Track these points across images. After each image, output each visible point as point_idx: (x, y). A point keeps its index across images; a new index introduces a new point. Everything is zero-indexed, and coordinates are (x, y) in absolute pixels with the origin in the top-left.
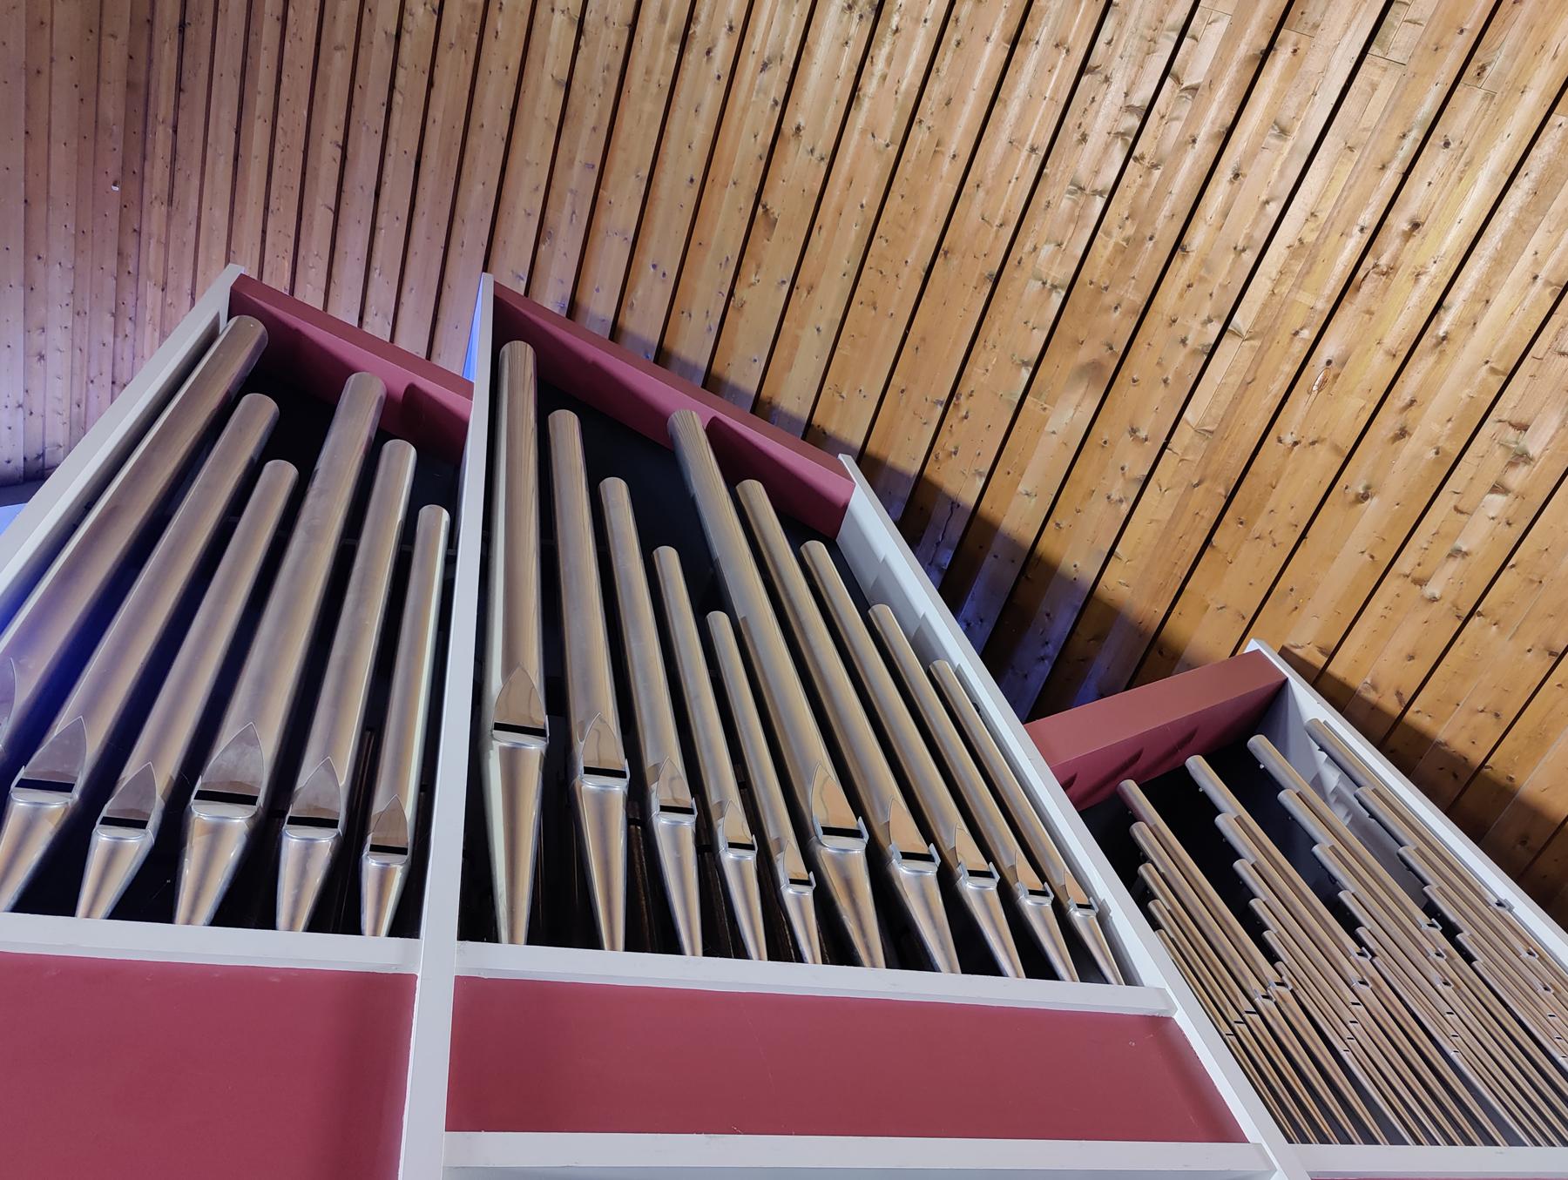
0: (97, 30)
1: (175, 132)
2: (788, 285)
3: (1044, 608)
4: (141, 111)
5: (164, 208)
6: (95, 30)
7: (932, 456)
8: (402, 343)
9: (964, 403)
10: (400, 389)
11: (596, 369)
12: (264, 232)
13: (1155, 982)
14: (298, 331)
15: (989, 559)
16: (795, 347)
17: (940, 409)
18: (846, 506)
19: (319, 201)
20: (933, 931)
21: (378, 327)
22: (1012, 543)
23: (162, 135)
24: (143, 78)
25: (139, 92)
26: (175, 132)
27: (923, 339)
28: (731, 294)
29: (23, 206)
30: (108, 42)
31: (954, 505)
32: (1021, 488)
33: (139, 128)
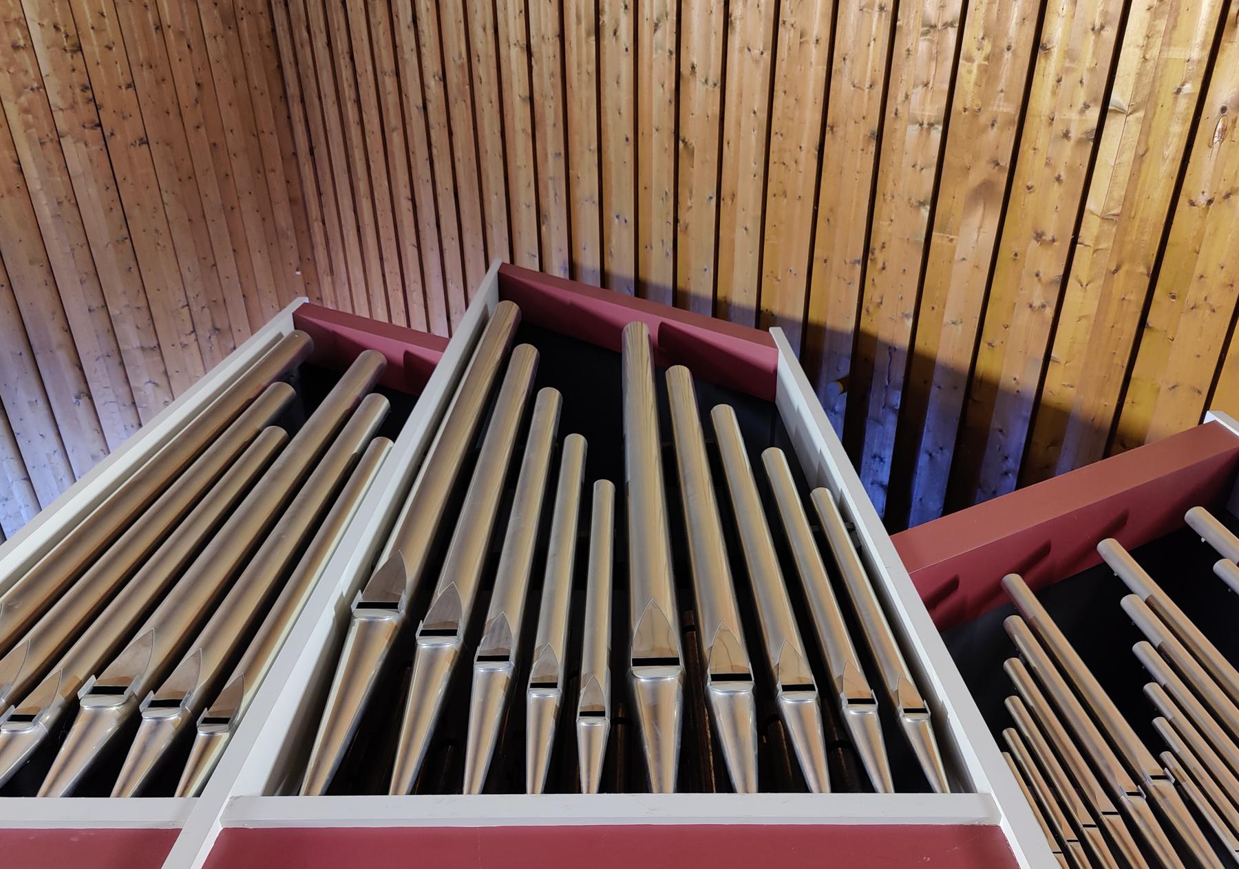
1: (324, 224)
3: (995, 424)
6: (261, 170)
7: (864, 311)
9: (879, 256)
10: (399, 357)
12: (384, 276)
14: (334, 334)
15: (934, 391)
17: (859, 267)
18: (775, 371)
21: (381, 316)
22: (951, 372)
23: (317, 227)
24: (300, 194)
26: (324, 224)
27: (831, 210)
28: (676, 221)
30: (270, 175)
31: (891, 349)
33: (304, 227)
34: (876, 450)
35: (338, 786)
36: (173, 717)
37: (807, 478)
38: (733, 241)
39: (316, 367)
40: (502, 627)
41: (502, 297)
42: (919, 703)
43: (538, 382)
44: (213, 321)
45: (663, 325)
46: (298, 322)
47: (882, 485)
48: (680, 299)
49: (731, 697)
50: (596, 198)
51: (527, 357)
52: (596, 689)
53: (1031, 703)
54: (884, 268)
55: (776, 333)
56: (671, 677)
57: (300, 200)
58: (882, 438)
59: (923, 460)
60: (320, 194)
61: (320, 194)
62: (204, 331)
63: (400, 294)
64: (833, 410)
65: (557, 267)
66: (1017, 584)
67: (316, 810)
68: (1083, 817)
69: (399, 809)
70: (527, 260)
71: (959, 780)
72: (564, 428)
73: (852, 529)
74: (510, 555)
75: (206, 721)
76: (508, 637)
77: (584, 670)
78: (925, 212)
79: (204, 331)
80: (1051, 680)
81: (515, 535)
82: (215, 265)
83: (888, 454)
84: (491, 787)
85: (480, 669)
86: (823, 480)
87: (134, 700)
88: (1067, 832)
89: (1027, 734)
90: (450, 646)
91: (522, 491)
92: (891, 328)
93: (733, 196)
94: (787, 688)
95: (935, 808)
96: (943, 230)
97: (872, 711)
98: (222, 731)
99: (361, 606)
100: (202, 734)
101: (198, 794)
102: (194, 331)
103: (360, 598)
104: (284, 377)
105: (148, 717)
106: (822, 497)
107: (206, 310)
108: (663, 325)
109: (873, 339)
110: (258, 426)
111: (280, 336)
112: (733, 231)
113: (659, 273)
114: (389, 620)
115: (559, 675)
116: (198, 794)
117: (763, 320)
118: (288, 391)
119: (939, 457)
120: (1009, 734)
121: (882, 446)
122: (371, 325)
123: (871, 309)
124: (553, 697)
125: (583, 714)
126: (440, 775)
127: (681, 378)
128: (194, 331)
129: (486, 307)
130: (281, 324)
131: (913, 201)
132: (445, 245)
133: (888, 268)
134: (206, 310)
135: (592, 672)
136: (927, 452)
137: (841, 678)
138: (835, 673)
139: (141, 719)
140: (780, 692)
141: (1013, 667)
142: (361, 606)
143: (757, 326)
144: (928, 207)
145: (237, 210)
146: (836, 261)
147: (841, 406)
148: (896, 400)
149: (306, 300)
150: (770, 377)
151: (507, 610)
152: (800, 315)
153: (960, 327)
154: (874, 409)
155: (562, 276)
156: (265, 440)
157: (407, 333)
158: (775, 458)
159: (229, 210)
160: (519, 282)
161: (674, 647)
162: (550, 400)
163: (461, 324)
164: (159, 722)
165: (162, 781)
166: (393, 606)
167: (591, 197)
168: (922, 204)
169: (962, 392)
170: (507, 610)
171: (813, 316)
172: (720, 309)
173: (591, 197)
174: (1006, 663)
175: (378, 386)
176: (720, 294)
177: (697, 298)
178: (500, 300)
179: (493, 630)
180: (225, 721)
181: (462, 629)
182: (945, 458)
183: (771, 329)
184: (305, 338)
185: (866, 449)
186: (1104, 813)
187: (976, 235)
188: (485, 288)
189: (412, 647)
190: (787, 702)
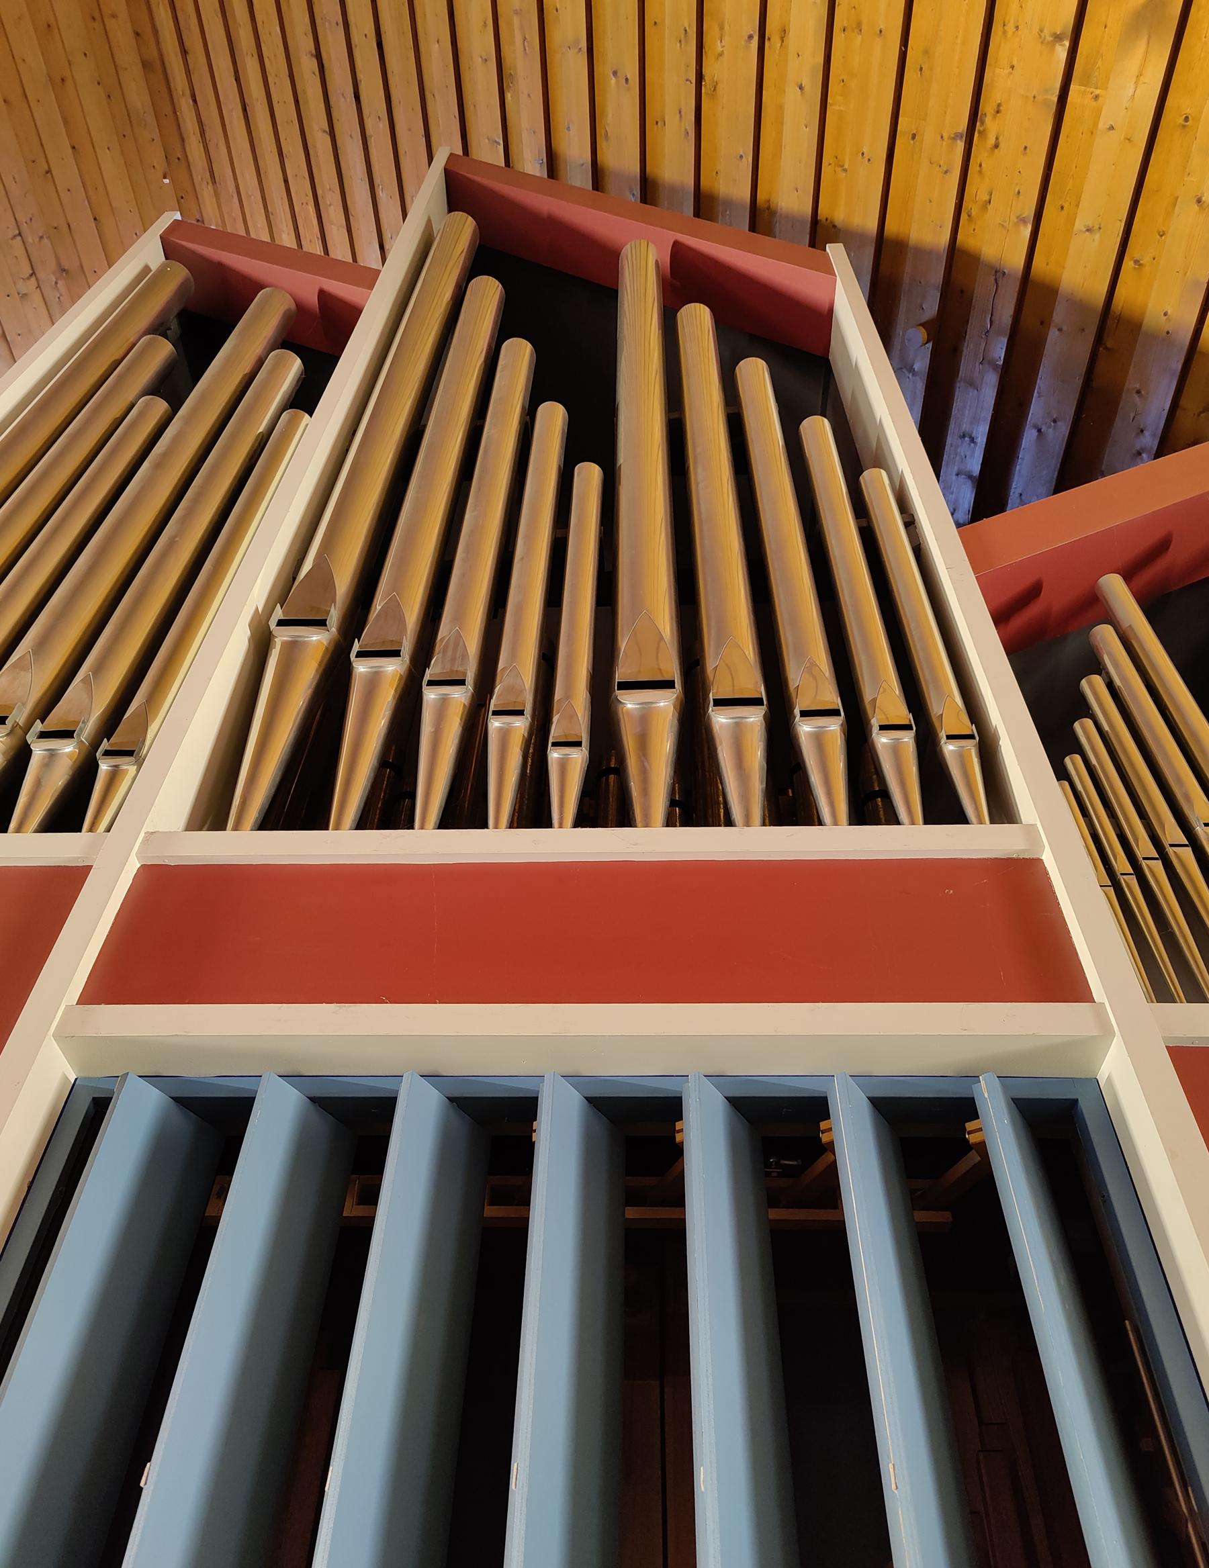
0: (97, 15)
1: (195, 101)
2: (756, 38)
3: (1132, 383)
4: (164, 89)
5: (210, 187)
6: (97, 16)
7: (964, 216)
8: (307, 247)
9: (990, 125)
10: (312, 300)
11: (553, 224)
12: (286, 181)
13: (1044, 825)
14: (220, 265)
15: (1053, 335)
16: (780, 123)
17: (960, 145)
18: (831, 311)
19: (316, 128)
20: (827, 777)
21: (287, 239)
22: (1078, 306)
23: (185, 104)
24: (155, 53)
25: (154, 68)
26: (195, 101)
27: (926, 52)
28: (700, 77)
29: (93, 224)
30: (111, 24)
31: (998, 273)
32: (1079, 225)
33: (168, 109)
34: (965, 427)
35: (272, 820)
36: (68, 749)
37: (856, 457)
38: (781, 108)
39: (200, 319)
40: (456, 644)
41: (452, 206)
42: (968, 727)
43: (504, 331)
44: (57, 258)
45: (676, 244)
46: (170, 250)
47: (970, 477)
48: (704, 205)
49: (737, 724)
50: (584, 44)
51: (487, 294)
52: (572, 716)
53: (1106, 727)
54: (996, 146)
55: (836, 252)
56: (665, 703)
57: (158, 63)
58: (974, 410)
59: (1029, 437)
60: (184, 52)
61: (184, 52)
62: (47, 274)
63: (311, 209)
64: (911, 370)
65: (531, 162)
66: (1116, 588)
67: (246, 846)
68: (1144, 847)
69: (341, 845)
70: (488, 151)
71: (1001, 808)
72: (537, 395)
73: (910, 523)
74: (467, 551)
75: (107, 753)
76: (465, 655)
77: (558, 694)
78: (1062, 52)
79: (47, 274)
80: (1135, 699)
81: (472, 532)
82: (49, 171)
83: (981, 432)
84: (447, 821)
85: (431, 695)
86: (881, 460)
87: (19, 732)
88: (1121, 864)
89: (1094, 761)
90: (393, 669)
91: (480, 479)
92: (1000, 242)
93: (784, 32)
94: (804, 714)
95: (975, 840)
96: (1086, 82)
97: (908, 739)
98: (128, 764)
99: (281, 623)
100: (104, 767)
101: (108, 830)
102: (33, 273)
103: (279, 613)
104: (158, 328)
105: (39, 750)
106: (875, 481)
107: (45, 241)
108: (676, 244)
109: (973, 259)
110: (131, 397)
111: (146, 269)
112: (781, 91)
113: (674, 167)
114: (318, 640)
115: (528, 701)
116: (108, 830)
117: (819, 232)
118: (164, 350)
119: (1050, 432)
120: (1073, 763)
121: (975, 420)
122: (271, 252)
123: (974, 213)
124: (520, 725)
125: (555, 744)
126: (390, 806)
127: (697, 320)
128: (33, 273)
129: (429, 222)
130: (147, 253)
131: (1046, 33)
132: (370, 130)
133: (1001, 145)
134: (45, 241)
135: (568, 696)
136: (1035, 427)
137: (874, 701)
138: (868, 694)
139: (30, 751)
140: (798, 718)
141: (1093, 688)
142: (281, 623)
143: (813, 244)
144: (1067, 43)
145: (69, 82)
146: (929, 136)
147: (922, 363)
148: (999, 351)
149: (178, 216)
150: (822, 320)
151: (464, 627)
152: (872, 225)
153: (1097, 236)
154: (967, 365)
155: (538, 174)
156: (141, 414)
157: (324, 263)
158: (818, 432)
159: (59, 83)
160: (473, 181)
161: (671, 668)
162: (519, 356)
163: (399, 252)
164: (52, 754)
165: (67, 815)
166: (321, 623)
167: (577, 41)
168: (1058, 38)
169: (1091, 337)
170: (464, 627)
171: (891, 227)
172: (760, 218)
173: (577, 41)
174: (1084, 682)
175: (287, 340)
176: (761, 196)
177: (729, 203)
178: (450, 211)
179: (446, 647)
180: (130, 753)
181: (407, 648)
182: (1058, 434)
183: (829, 248)
184: (180, 273)
185: (952, 426)
186: (1171, 845)
187: (1132, 86)
188: (428, 191)
189: (348, 670)
190: (805, 729)
